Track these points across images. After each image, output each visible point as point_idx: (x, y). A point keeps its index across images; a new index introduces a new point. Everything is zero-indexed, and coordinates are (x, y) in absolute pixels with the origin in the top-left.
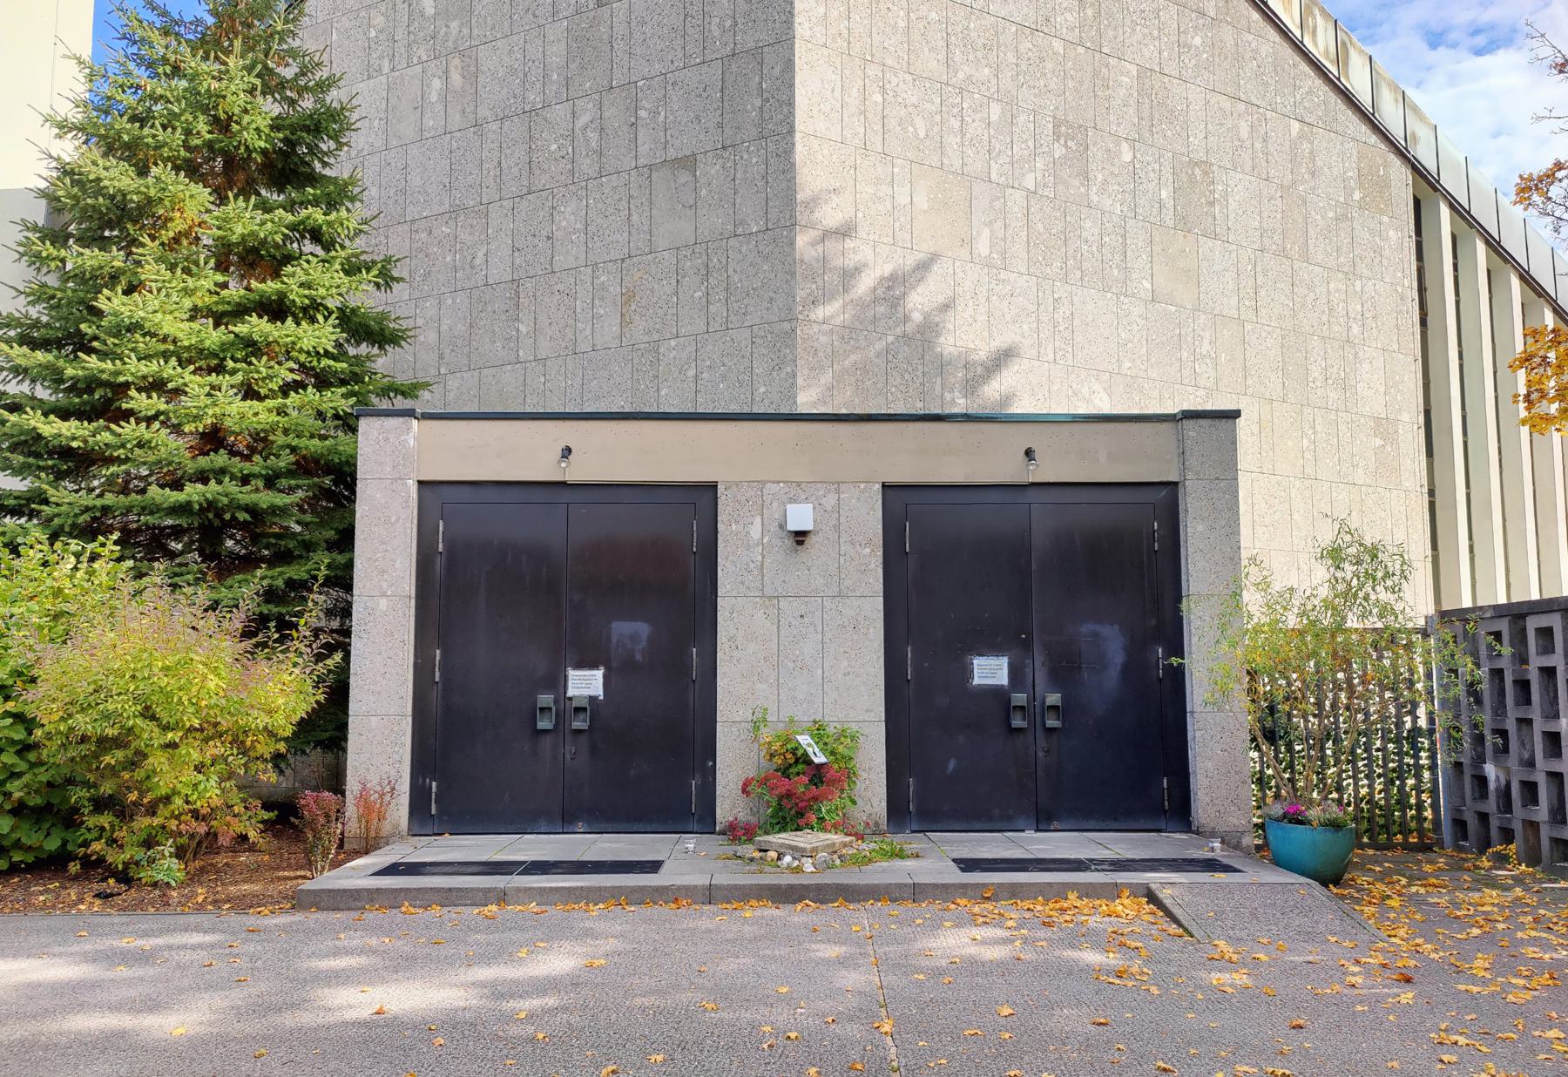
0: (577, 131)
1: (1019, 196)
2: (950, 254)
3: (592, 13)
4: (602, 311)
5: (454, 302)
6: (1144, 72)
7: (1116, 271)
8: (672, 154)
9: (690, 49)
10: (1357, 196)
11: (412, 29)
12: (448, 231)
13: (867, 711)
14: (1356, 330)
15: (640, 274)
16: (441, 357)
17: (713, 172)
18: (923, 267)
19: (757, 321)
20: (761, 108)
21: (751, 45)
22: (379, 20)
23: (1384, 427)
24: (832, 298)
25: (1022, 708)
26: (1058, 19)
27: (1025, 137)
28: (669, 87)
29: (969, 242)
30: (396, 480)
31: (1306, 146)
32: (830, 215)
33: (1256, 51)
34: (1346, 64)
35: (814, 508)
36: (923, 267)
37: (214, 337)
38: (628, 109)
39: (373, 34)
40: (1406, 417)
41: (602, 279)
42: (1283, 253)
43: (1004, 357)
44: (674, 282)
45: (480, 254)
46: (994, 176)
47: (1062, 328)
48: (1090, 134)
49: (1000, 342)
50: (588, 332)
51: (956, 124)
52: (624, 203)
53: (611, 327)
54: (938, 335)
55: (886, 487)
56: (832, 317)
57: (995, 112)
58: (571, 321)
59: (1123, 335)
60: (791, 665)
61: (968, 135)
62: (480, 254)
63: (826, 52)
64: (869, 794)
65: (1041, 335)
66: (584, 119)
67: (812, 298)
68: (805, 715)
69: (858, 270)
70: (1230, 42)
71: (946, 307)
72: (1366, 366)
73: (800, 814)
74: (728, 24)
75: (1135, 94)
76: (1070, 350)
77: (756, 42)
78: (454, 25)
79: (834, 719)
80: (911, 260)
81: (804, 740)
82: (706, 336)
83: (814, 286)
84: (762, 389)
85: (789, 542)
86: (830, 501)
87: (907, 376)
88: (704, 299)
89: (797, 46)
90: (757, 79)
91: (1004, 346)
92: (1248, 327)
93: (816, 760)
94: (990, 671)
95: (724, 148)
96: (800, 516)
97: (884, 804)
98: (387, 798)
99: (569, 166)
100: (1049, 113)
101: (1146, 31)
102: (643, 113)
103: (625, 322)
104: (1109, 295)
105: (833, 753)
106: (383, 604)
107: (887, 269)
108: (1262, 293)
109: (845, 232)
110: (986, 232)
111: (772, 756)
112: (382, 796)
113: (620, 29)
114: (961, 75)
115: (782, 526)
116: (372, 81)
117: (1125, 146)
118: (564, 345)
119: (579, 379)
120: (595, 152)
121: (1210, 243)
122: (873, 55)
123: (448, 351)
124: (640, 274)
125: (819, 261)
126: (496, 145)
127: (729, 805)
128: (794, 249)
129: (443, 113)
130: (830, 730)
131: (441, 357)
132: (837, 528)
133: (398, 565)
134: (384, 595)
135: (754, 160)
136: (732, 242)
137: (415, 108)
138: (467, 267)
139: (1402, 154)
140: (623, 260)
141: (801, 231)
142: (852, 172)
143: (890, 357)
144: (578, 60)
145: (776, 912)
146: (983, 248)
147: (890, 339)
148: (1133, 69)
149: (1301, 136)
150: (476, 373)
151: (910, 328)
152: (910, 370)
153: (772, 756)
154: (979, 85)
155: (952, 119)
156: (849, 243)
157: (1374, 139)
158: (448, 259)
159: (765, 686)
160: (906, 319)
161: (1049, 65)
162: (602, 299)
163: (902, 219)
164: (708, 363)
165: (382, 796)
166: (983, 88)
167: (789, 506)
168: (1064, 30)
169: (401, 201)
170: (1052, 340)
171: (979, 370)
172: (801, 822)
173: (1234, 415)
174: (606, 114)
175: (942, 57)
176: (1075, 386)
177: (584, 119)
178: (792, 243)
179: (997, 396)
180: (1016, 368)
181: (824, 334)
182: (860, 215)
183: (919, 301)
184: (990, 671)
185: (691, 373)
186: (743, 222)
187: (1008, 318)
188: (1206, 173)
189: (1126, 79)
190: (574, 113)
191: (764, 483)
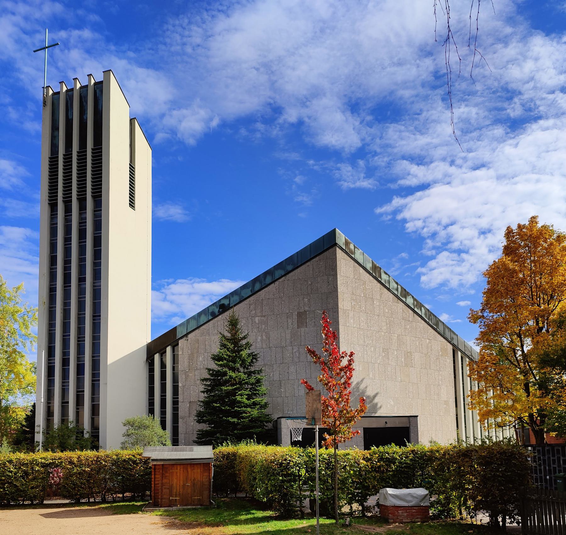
1: (376, 365)
6: (399, 336)
9: (318, 340)
10: (440, 353)
14: (440, 382)
18: (362, 381)
23: (446, 403)
29: (369, 375)
31: (430, 344)
33: (420, 326)
34: (438, 325)
36: (362, 381)
40: (451, 400)
42: (426, 368)
49: (375, 392)
51: (366, 352)
52: (304, 368)
55: (364, 428)
57: (372, 349)
66: (295, 351)
70: (415, 326)
71: (366, 387)
72: (443, 390)
78: (263, 326)
92: (419, 385)
108: (422, 377)
110: (371, 373)
113: (302, 334)
121: (411, 368)
126: (275, 352)
139: (450, 342)
146: (371, 376)
148: (396, 335)
149: (429, 343)
157: (444, 340)
161: (381, 338)
173: (417, 416)
174: (300, 350)
183: (362, 387)
188: (410, 354)
189: (395, 337)
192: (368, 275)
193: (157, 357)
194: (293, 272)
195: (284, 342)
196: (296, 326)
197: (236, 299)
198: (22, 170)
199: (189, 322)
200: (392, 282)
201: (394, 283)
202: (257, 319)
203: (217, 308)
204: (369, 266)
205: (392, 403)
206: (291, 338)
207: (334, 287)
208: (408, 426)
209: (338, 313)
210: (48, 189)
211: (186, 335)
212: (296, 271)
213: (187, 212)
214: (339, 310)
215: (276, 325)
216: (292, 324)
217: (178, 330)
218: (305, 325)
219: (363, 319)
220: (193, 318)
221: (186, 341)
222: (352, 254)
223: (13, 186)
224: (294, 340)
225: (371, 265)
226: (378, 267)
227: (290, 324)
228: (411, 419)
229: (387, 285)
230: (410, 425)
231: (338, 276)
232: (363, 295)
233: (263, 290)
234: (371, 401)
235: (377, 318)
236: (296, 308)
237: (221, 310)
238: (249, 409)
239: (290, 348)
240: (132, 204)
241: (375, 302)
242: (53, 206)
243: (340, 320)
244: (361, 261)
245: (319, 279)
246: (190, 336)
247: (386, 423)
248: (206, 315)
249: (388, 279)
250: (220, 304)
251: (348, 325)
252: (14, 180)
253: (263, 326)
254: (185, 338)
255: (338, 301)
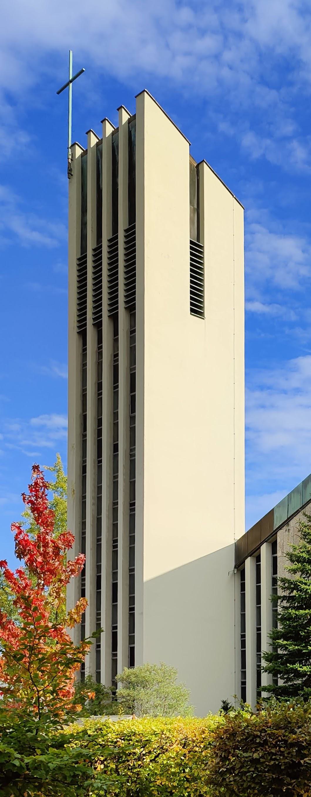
193: (249, 563)
199: (291, 499)
210: (76, 316)
211: (286, 523)
217: (276, 515)
220: (296, 491)
221: (287, 533)
242: (83, 334)
246: (292, 523)
254: (285, 528)
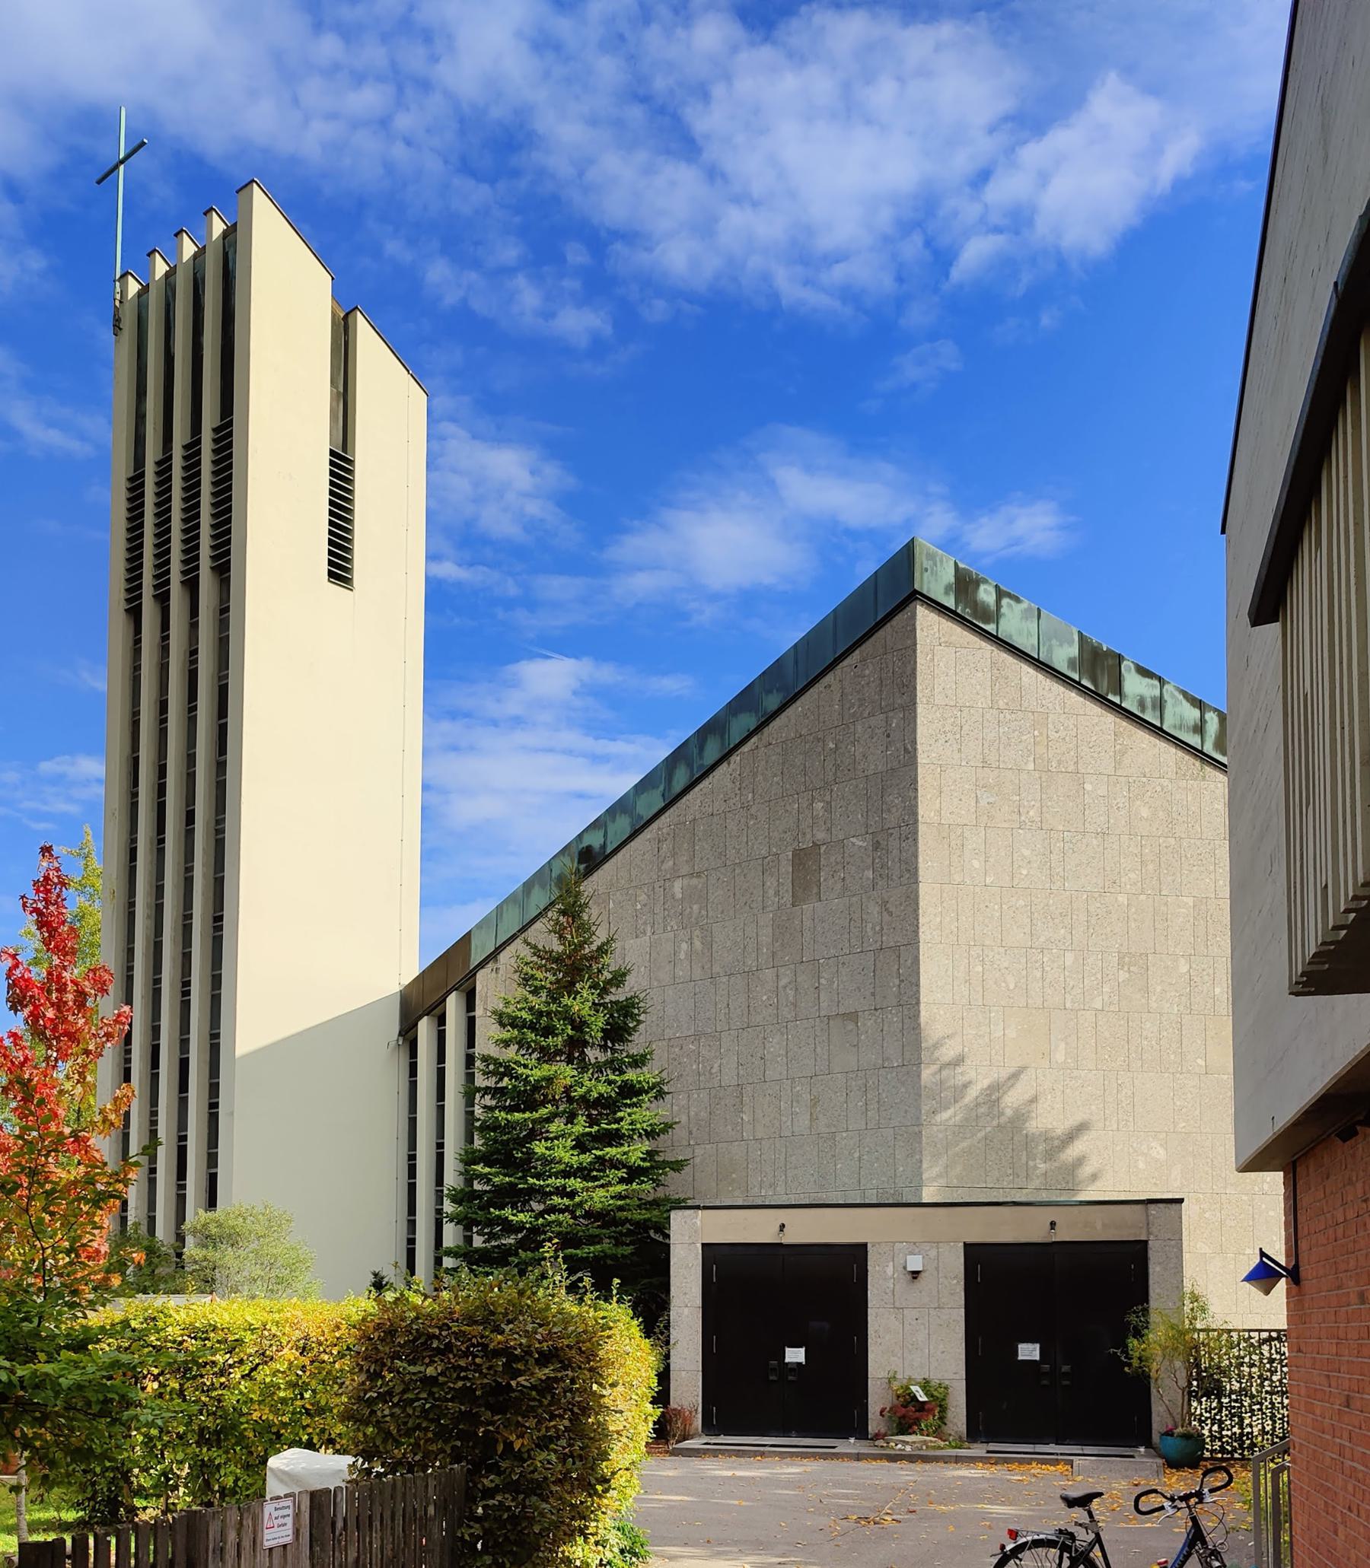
0: (780, 989)
2: (1033, 1065)
3: (788, 911)
4: (797, 1110)
5: (699, 1096)
7: (1172, 1057)
8: (842, 1011)
11: (666, 907)
12: (694, 1048)
13: (955, 1373)
15: (822, 1087)
16: (690, 1133)
17: (869, 1024)
18: (1015, 1076)
19: (897, 1124)
20: (899, 986)
21: (892, 944)
22: (643, 898)
24: (947, 1108)
25: (775, 1369)
26: (1123, 880)
27: (1094, 971)
28: (840, 966)
30: (690, 1244)
32: (948, 1053)
35: (923, 1257)
36: (1015, 1076)
37: (587, 1158)
38: (813, 977)
39: (639, 907)
41: (798, 1088)
43: (1081, 1128)
44: (845, 1094)
45: (716, 1065)
46: (1068, 1005)
47: (1124, 1105)
48: (1150, 958)
50: (789, 1123)
52: (811, 1039)
53: (804, 1121)
54: (1025, 1121)
56: (947, 1120)
57: (1069, 958)
58: (778, 1116)
59: (1178, 1103)
60: (910, 1347)
61: (1048, 981)
62: (716, 1065)
63: (941, 946)
64: (955, 1420)
65: (1107, 1111)
66: (783, 982)
67: (933, 1110)
68: (919, 1376)
69: (966, 1086)
71: (1034, 1100)
73: (910, 1427)
74: (878, 928)
75: (1192, 920)
76: (1131, 1119)
77: (895, 942)
78: (695, 907)
79: (935, 1378)
80: (1004, 1074)
81: (916, 1390)
82: (866, 1132)
83: (934, 1102)
84: (901, 1169)
85: (909, 1277)
86: (933, 1253)
87: (1000, 1153)
88: (864, 1107)
89: (921, 947)
90: (896, 967)
91: (1076, 1123)
93: (920, 1399)
94: (1029, 1352)
95: (875, 1009)
96: (915, 1263)
97: (965, 1426)
98: (694, 1414)
99: (775, 1012)
100: (1115, 950)
101: (1202, 868)
102: (823, 981)
103: (813, 1119)
104: (1167, 1075)
105: (932, 1396)
106: (686, 1311)
107: (986, 1083)
109: (959, 1061)
110: (1062, 1045)
111: (898, 1397)
112: (691, 1412)
113: (807, 923)
114: (1042, 939)
115: (905, 1268)
116: (638, 940)
117: (1182, 961)
118: (773, 1130)
119: (783, 1154)
120: (792, 1004)
122: (975, 941)
123: (695, 1129)
124: (822, 1087)
125: (937, 1085)
126: (726, 992)
127: (875, 1424)
128: (920, 1079)
129: (689, 967)
130: (932, 1384)
131: (690, 1133)
132: (937, 1269)
133: (693, 1290)
134: (687, 1306)
135: (895, 1019)
136: (882, 1071)
137: (670, 962)
138: (707, 1074)
140: (811, 1077)
141: (925, 1068)
142: (961, 1021)
143: (988, 1141)
144: (780, 941)
145: (887, 1463)
146: (1060, 1057)
147: (989, 1129)
148: (1190, 901)
150: (714, 1146)
151: (1003, 1120)
152: (1002, 1148)
153: (898, 1397)
154: (1057, 942)
155: (1035, 971)
156: (959, 1070)
158: (694, 1067)
159: (896, 1358)
160: (1001, 1114)
162: (798, 1102)
163: (997, 1047)
164: (867, 1149)
165: (691, 1412)
166: (1060, 944)
167: (908, 1257)
168: (1128, 886)
169: (661, 1025)
170: (1115, 1115)
171: (1056, 1143)
172: (910, 1431)
173: (1181, 1201)
175: (1027, 930)
176: (1135, 1145)
177: (783, 982)
178: (919, 1076)
179: (1070, 1159)
180: (1085, 1138)
181: (941, 1132)
182: (966, 1049)
183: (1012, 1099)
184: (1029, 1352)
185: (857, 1155)
186: (888, 1059)
187: (1079, 1103)
190: (777, 976)
191: (894, 1243)
192: (1062, 689)
193: (425, 1028)
194: (783, 716)
195: (754, 955)
196: (788, 898)
197: (622, 826)
198: (552, 472)
199: (501, 915)
200: (1177, 703)
201: (1186, 705)
202: (677, 887)
203: (572, 862)
204: (1063, 655)
205: (1159, 1153)
206: (775, 940)
207: (906, 749)
208: (1143, 1238)
209: (916, 840)
211: (493, 956)
212: (790, 711)
213: (1072, 519)
214: (922, 828)
215: (731, 899)
216: (777, 893)
218: (815, 890)
219: (1027, 853)
220: (512, 899)
222: (987, 621)
223: (531, 525)
224: (782, 945)
225: (1074, 651)
226: (1110, 653)
227: (771, 892)
228: (1153, 1209)
229: (1150, 716)
230: (1149, 1233)
231: (920, 709)
232: (1031, 766)
233: (697, 789)
234: (1050, 1155)
235: (1095, 842)
236: (788, 837)
237: (582, 867)
238: (575, 1183)
239: (769, 973)
240: (340, 571)
241: (1088, 787)
242: (134, 613)
243: (921, 865)
244: (1027, 644)
245: (859, 728)
247: (1053, 1224)
248: (543, 886)
249: (1157, 693)
250: (581, 846)
251: (957, 878)
252: (533, 508)
253: (695, 907)
255: (916, 798)
